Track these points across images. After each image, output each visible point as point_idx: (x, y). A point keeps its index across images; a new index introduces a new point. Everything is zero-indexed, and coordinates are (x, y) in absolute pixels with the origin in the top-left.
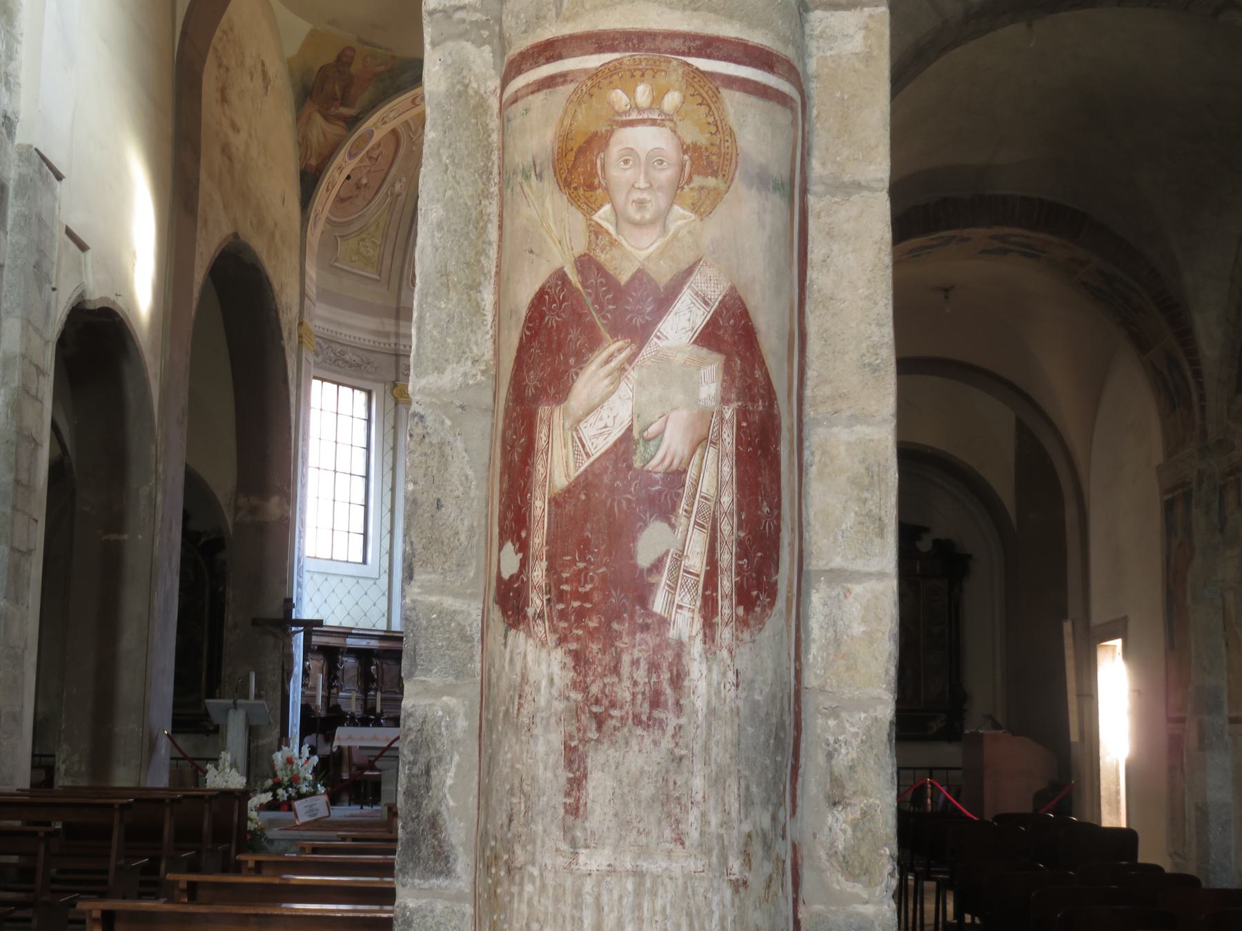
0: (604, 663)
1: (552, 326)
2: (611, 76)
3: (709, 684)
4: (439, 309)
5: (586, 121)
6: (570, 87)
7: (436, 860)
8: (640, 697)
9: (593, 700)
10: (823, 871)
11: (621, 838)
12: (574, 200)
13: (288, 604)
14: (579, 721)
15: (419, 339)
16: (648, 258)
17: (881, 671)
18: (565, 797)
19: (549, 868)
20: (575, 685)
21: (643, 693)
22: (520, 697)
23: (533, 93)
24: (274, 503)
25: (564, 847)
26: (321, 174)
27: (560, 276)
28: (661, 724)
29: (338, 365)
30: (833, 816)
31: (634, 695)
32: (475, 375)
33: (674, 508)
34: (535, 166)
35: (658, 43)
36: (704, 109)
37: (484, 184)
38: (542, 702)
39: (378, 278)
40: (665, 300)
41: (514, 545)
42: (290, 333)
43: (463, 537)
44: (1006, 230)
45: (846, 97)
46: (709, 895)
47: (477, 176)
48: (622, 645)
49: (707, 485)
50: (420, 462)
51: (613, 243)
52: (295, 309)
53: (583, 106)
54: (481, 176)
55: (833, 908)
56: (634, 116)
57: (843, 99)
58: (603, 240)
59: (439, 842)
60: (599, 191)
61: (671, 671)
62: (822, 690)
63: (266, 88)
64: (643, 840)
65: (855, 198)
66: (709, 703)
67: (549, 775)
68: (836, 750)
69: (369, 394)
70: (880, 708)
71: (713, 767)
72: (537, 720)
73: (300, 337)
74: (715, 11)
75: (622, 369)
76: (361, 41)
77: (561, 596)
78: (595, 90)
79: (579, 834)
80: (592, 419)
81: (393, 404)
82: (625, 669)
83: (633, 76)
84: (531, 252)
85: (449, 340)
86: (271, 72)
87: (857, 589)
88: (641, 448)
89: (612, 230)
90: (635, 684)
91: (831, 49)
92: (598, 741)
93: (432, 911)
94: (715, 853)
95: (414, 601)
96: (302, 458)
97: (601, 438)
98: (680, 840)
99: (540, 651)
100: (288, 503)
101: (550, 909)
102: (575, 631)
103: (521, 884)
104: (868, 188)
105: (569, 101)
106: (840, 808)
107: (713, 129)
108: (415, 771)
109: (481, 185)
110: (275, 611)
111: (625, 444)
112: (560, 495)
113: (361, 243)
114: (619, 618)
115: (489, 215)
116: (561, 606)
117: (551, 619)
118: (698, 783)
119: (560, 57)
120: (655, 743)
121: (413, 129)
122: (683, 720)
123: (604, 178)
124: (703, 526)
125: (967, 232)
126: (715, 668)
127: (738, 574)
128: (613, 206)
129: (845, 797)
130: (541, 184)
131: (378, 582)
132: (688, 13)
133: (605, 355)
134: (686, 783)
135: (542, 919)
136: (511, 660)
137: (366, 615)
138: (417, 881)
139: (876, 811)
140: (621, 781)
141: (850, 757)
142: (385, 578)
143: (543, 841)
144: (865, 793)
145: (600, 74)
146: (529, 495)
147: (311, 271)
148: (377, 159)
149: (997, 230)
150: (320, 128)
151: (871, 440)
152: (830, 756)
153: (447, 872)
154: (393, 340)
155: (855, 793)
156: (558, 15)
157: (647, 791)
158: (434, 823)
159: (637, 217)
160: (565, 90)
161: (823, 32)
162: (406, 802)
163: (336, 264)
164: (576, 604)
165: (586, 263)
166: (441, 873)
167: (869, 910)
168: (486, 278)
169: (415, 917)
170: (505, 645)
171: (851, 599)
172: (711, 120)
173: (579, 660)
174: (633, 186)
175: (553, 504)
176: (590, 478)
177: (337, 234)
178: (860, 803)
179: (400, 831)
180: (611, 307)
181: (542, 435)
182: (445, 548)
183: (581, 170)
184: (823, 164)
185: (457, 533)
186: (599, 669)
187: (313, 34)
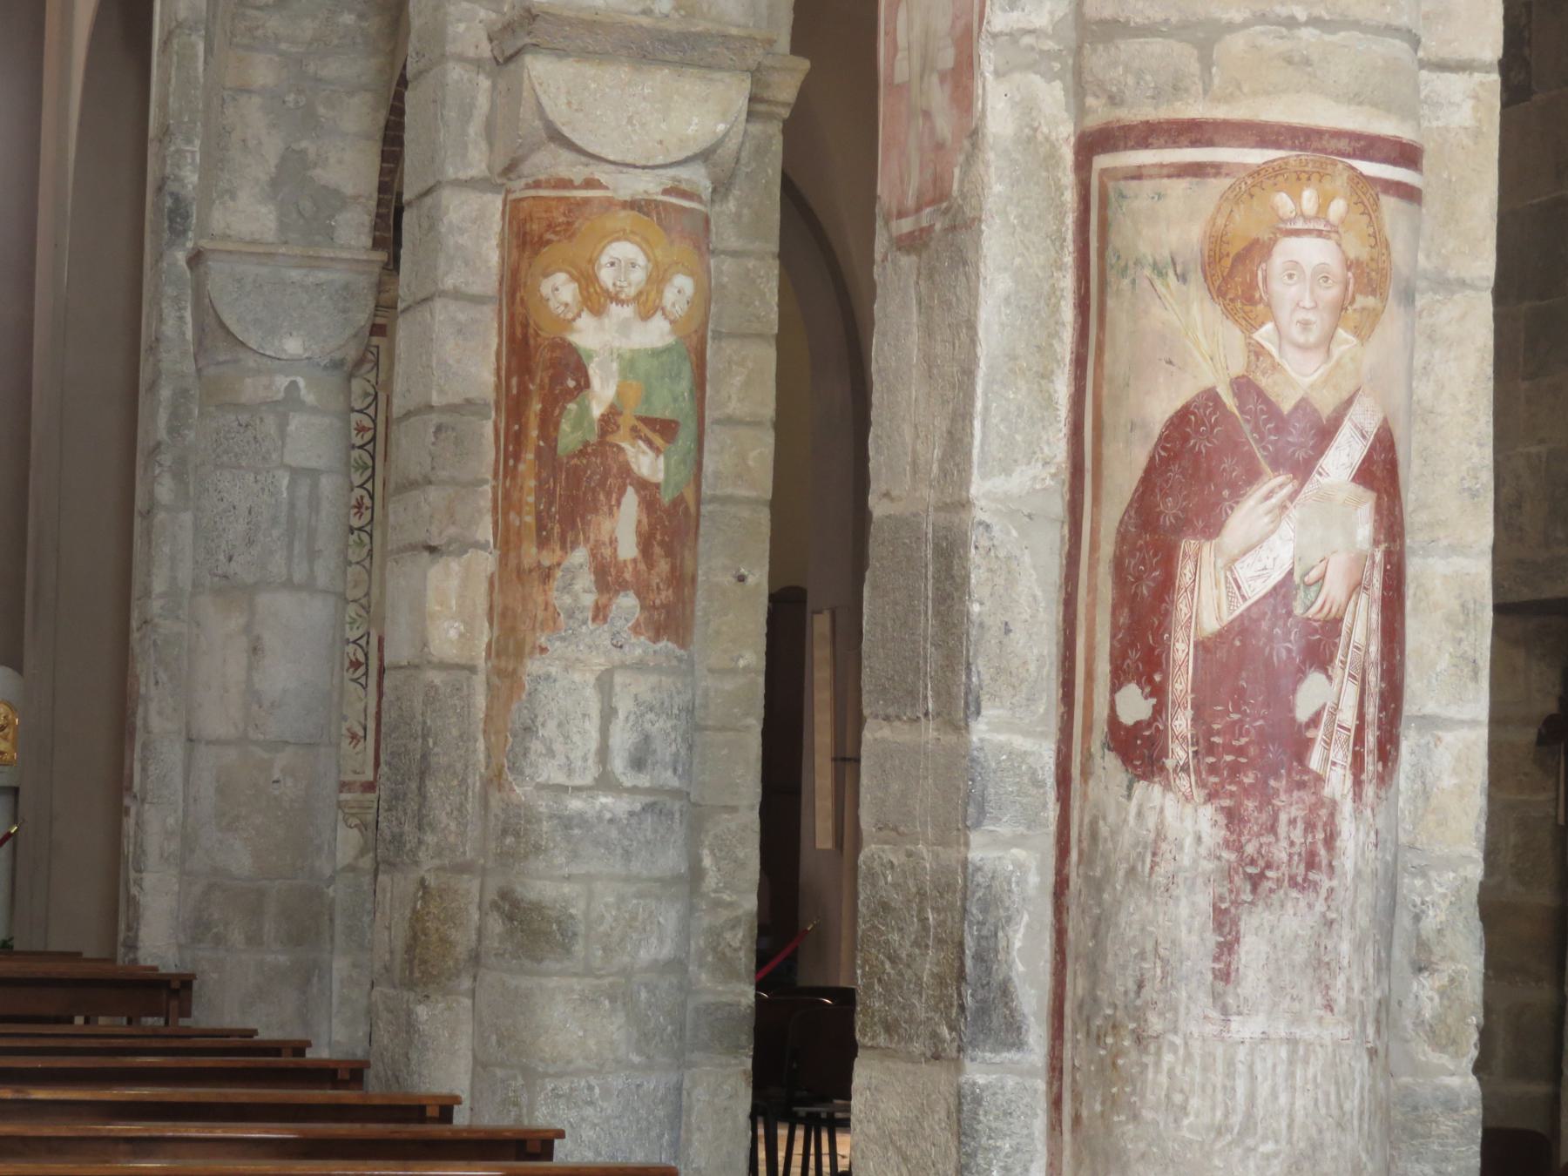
0: (1260, 821)
1: (1200, 452)
2: (1276, 176)
3: (1357, 845)
4: (1007, 399)
5: (1245, 224)
6: (1226, 182)
7: (1007, 1031)
8: (1296, 857)
9: (1248, 860)
10: (1407, 1041)
11: (1275, 1005)
12: (1230, 313)
14: (1231, 882)
15: (984, 435)
16: (1312, 386)
17: (1472, 827)
18: (1214, 961)
19: (1196, 1036)
20: (1227, 844)
21: (1300, 854)
22: (1154, 854)
23: (1169, 176)
25: (1215, 1014)
27: (1211, 396)
28: (1315, 886)
30: (1419, 983)
31: (1290, 856)
32: (1044, 479)
33: (1331, 660)
34: (1174, 264)
35: (1324, 142)
36: (1365, 218)
37: (1057, 252)
38: (1186, 861)
40: (1325, 433)
41: (1142, 689)
43: (1032, 667)
45: (1454, 179)
46: (1353, 1063)
47: (1049, 241)
48: (1279, 804)
49: (1359, 636)
50: (987, 579)
51: (1275, 367)
53: (1242, 206)
54: (1053, 242)
55: (1421, 1081)
56: (1300, 225)
57: (1450, 181)
58: (1265, 363)
59: (1011, 1012)
60: (1261, 307)
61: (1325, 831)
62: (1412, 847)
64: (1296, 1006)
65: (1457, 297)
66: (1356, 864)
67: (1195, 938)
68: (1423, 912)
70: (1470, 867)
71: (1358, 932)
72: (1180, 879)
74: (1375, 105)
75: (1283, 507)
77: (1211, 749)
78: (1256, 190)
79: (1230, 1000)
80: (1249, 559)
82: (1282, 828)
83: (1299, 179)
84: (1170, 362)
85: (1019, 438)
87: (1448, 737)
88: (1301, 594)
89: (1274, 351)
90: (1292, 844)
91: (1438, 119)
92: (1252, 903)
93: (1002, 1088)
94: (1358, 1019)
95: (982, 740)
97: (1259, 581)
98: (1329, 1007)
99: (1183, 806)
101: (1198, 1079)
102: (1228, 787)
103: (1158, 1053)
104: (1473, 287)
105: (1223, 197)
106: (1426, 974)
107: (1372, 241)
108: (985, 932)
109: (1053, 253)
111: (1283, 590)
112: (1209, 639)
114: (1277, 777)
115: (1062, 290)
116: (1211, 760)
117: (1198, 772)
118: (1345, 947)
119: (1210, 143)
120: (1310, 906)
122: (1335, 883)
123: (1266, 292)
124: (1354, 678)
126: (1361, 827)
127: (1379, 728)
128: (1276, 325)
129: (1432, 963)
130: (1184, 288)
132: (1352, 108)
133: (1265, 489)
134: (1335, 948)
135: (1186, 1088)
136: (1140, 814)
138: (988, 1055)
139: (1124, 967)
140: (1275, 946)
141: (1438, 919)
143: (1188, 1008)
144: (1452, 958)
145: (1263, 173)
146: (1166, 636)
151: (1468, 574)
152: (1417, 918)
153: (1019, 1045)
155: (1443, 958)
156: (1206, 92)
157: (1301, 955)
158: (1005, 990)
159: (1301, 339)
160: (1218, 185)
161: (1427, 97)
162: (975, 966)
164: (1229, 758)
165: (1244, 387)
166: (1013, 1045)
167: (1455, 1082)
168: (1059, 366)
169: (984, 1094)
170: (1129, 797)
171: (1441, 748)
172: (1371, 231)
173: (1233, 817)
174: (1298, 304)
175: (1200, 648)
176: (1246, 622)
178: (1448, 968)
179: (969, 999)
180: (1273, 438)
181: (1187, 571)
182: (1014, 680)
183: (1238, 279)
184: (1428, 256)
185: (1025, 663)
186: (1256, 828)
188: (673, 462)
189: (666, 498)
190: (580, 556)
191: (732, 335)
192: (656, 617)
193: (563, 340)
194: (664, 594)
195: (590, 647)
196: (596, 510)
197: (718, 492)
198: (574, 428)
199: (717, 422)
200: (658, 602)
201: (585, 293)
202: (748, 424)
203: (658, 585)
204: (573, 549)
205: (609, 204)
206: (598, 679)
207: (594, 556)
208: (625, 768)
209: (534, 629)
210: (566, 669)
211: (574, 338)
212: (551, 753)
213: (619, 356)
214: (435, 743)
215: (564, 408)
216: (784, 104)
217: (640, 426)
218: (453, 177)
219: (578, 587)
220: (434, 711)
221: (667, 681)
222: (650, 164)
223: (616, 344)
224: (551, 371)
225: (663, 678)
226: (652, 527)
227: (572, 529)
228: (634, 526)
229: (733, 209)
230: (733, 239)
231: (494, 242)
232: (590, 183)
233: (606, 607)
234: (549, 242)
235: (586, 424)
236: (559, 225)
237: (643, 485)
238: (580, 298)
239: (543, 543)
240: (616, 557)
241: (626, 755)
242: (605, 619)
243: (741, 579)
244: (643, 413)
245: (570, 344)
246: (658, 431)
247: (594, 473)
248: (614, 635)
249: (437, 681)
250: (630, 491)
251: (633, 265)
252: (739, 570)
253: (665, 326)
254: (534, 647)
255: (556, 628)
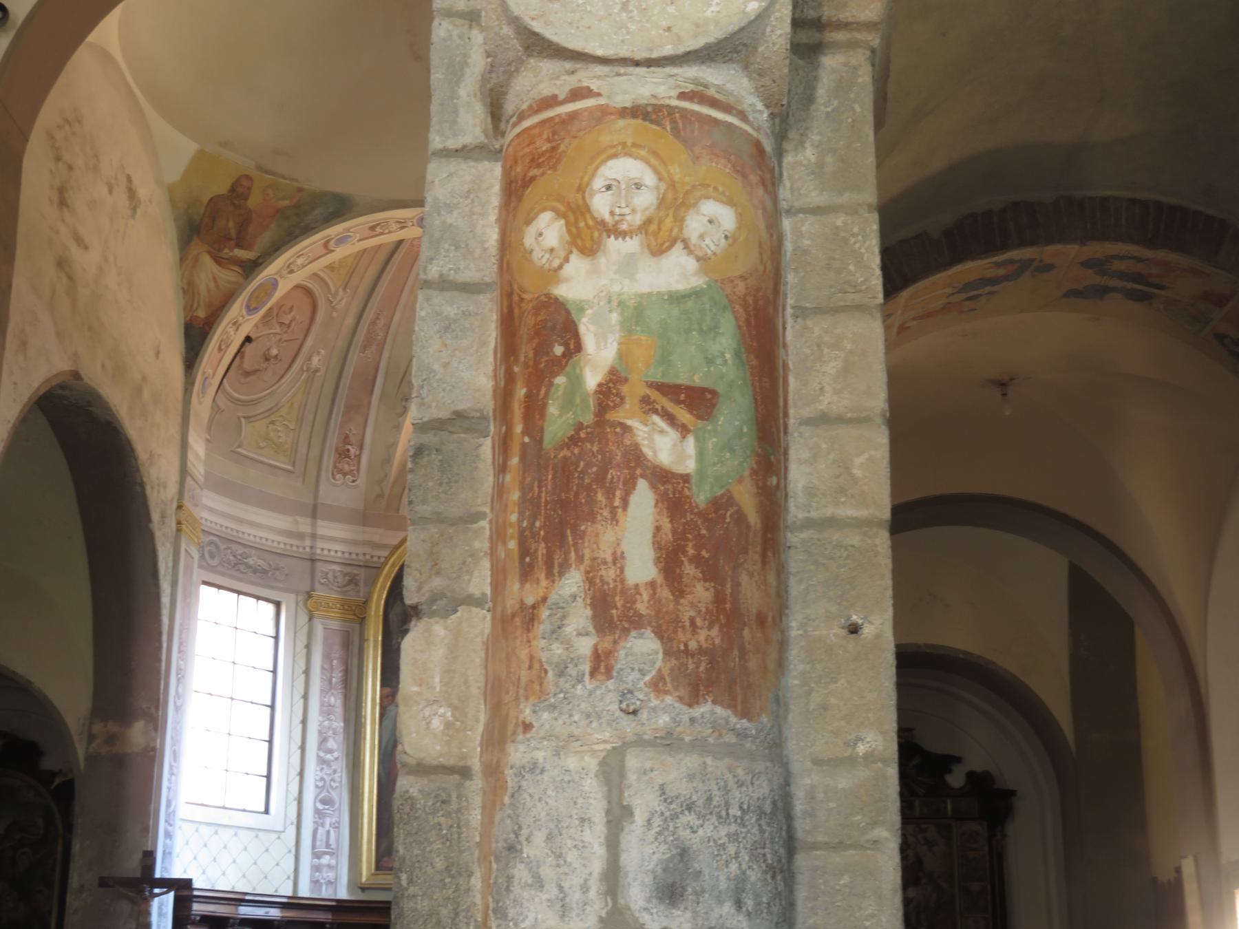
13: (149, 857)
24: (137, 732)
26: (210, 328)
29: (239, 570)
39: (290, 468)
42: (163, 516)
44: (1111, 248)
52: (172, 489)
63: (134, 209)
69: (278, 605)
73: (179, 523)
76: (260, 168)
81: (306, 618)
86: (143, 193)
96: (178, 674)
100: (156, 728)
110: (131, 867)
113: (271, 427)
121: (333, 289)
125: (1049, 252)
131: (282, 835)
137: (266, 877)
142: (292, 831)
147: (198, 446)
148: (289, 326)
149: (1097, 249)
150: (210, 275)
154: (308, 543)
163: (239, 450)
177: (240, 414)
187: (200, 156)
188: (710, 446)
189: (701, 497)
190: (572, 583)
191: (819, 311)
192: (691, 667)
193: (548, 296)
194: (702, 635)
195: (588, 716)
196: (592, 517)
197: (814, 514)
198: (564, 409)
199: (808, 422)
200: (693, 645)
201: (574, 230)
202: (850, 421)
203: (692, 621)
204: (561, 574)
205: (603, 113)
206: (603, 763)
207: (590, 581)
208: (649, 901)
209: (517, 699)
210: (557, 753)
211: (563, 291)
212: (538, 883)
213: (620, 303)
214: (410, 881)
215: (551, 384)
216: (870, 26)
217: (655, 395)
218: (440, 146)
219: (570, 629)
220: (409, 834)
221: (716, 766)
222: (655, 55)
223: (616, 288)
224: (536, 341)
225: (709, 760)
226: (680, 538)
227: (561, 547)
228: (649, 536)
229: (813, 159)
230: (814, 194)
231: (493, 217)
232: (577, 94)
233: (609, 653)
234: (533, 179)
235: (578, 400)
236: (543, 154)
237: (661, 477)
238: (567, 238)
239: (526, 573)
240: (623, 581)
241: (649, 879)
242: (608, 675)
243: (854, 630)
244: (659, 378)
245: (556, 299)
246: (683, 402)
247: (588, 465)
248: (626, 694)
249: (414, 792)
250: (642, 485)
251: (638, 186)
252: (849, 617)
253: (691, 264)
254: (517, 725)
255: (542, 694)
